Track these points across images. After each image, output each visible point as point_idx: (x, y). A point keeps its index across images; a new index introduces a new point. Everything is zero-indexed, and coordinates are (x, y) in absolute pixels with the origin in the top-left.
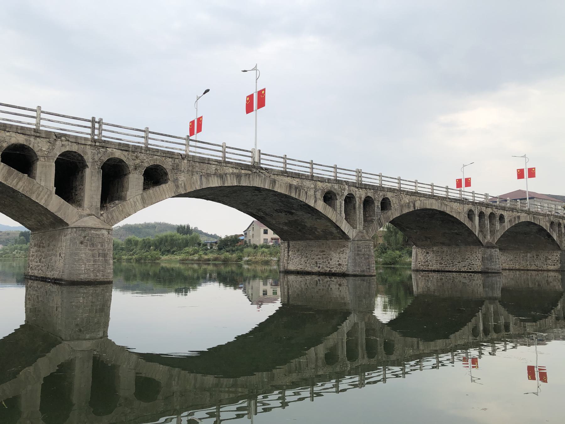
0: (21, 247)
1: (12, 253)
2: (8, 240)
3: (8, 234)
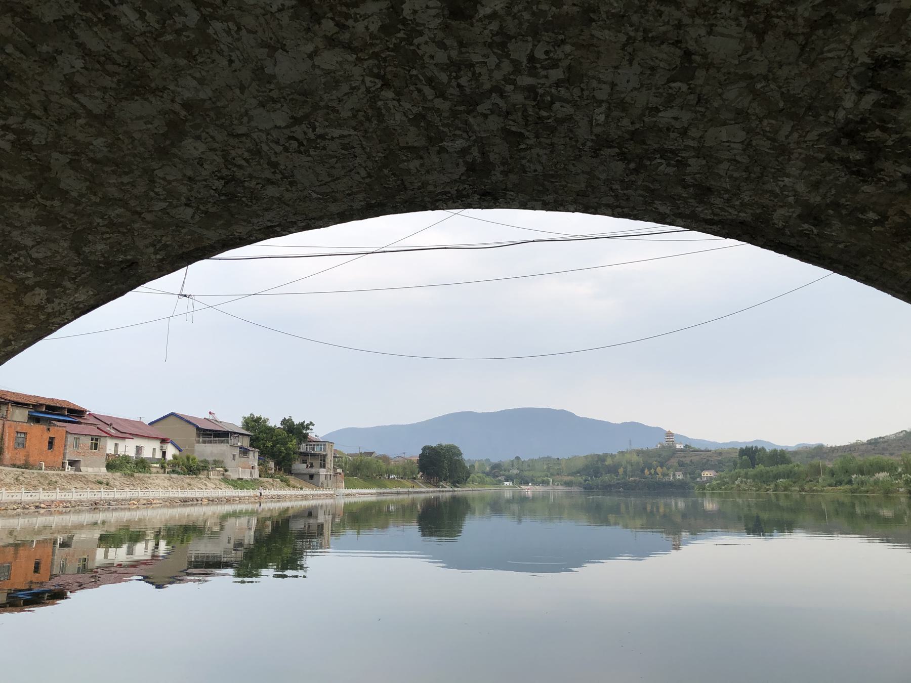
0: (746, 474)
1: (734, 483)
2: (720, 462)
3: (720, 454)
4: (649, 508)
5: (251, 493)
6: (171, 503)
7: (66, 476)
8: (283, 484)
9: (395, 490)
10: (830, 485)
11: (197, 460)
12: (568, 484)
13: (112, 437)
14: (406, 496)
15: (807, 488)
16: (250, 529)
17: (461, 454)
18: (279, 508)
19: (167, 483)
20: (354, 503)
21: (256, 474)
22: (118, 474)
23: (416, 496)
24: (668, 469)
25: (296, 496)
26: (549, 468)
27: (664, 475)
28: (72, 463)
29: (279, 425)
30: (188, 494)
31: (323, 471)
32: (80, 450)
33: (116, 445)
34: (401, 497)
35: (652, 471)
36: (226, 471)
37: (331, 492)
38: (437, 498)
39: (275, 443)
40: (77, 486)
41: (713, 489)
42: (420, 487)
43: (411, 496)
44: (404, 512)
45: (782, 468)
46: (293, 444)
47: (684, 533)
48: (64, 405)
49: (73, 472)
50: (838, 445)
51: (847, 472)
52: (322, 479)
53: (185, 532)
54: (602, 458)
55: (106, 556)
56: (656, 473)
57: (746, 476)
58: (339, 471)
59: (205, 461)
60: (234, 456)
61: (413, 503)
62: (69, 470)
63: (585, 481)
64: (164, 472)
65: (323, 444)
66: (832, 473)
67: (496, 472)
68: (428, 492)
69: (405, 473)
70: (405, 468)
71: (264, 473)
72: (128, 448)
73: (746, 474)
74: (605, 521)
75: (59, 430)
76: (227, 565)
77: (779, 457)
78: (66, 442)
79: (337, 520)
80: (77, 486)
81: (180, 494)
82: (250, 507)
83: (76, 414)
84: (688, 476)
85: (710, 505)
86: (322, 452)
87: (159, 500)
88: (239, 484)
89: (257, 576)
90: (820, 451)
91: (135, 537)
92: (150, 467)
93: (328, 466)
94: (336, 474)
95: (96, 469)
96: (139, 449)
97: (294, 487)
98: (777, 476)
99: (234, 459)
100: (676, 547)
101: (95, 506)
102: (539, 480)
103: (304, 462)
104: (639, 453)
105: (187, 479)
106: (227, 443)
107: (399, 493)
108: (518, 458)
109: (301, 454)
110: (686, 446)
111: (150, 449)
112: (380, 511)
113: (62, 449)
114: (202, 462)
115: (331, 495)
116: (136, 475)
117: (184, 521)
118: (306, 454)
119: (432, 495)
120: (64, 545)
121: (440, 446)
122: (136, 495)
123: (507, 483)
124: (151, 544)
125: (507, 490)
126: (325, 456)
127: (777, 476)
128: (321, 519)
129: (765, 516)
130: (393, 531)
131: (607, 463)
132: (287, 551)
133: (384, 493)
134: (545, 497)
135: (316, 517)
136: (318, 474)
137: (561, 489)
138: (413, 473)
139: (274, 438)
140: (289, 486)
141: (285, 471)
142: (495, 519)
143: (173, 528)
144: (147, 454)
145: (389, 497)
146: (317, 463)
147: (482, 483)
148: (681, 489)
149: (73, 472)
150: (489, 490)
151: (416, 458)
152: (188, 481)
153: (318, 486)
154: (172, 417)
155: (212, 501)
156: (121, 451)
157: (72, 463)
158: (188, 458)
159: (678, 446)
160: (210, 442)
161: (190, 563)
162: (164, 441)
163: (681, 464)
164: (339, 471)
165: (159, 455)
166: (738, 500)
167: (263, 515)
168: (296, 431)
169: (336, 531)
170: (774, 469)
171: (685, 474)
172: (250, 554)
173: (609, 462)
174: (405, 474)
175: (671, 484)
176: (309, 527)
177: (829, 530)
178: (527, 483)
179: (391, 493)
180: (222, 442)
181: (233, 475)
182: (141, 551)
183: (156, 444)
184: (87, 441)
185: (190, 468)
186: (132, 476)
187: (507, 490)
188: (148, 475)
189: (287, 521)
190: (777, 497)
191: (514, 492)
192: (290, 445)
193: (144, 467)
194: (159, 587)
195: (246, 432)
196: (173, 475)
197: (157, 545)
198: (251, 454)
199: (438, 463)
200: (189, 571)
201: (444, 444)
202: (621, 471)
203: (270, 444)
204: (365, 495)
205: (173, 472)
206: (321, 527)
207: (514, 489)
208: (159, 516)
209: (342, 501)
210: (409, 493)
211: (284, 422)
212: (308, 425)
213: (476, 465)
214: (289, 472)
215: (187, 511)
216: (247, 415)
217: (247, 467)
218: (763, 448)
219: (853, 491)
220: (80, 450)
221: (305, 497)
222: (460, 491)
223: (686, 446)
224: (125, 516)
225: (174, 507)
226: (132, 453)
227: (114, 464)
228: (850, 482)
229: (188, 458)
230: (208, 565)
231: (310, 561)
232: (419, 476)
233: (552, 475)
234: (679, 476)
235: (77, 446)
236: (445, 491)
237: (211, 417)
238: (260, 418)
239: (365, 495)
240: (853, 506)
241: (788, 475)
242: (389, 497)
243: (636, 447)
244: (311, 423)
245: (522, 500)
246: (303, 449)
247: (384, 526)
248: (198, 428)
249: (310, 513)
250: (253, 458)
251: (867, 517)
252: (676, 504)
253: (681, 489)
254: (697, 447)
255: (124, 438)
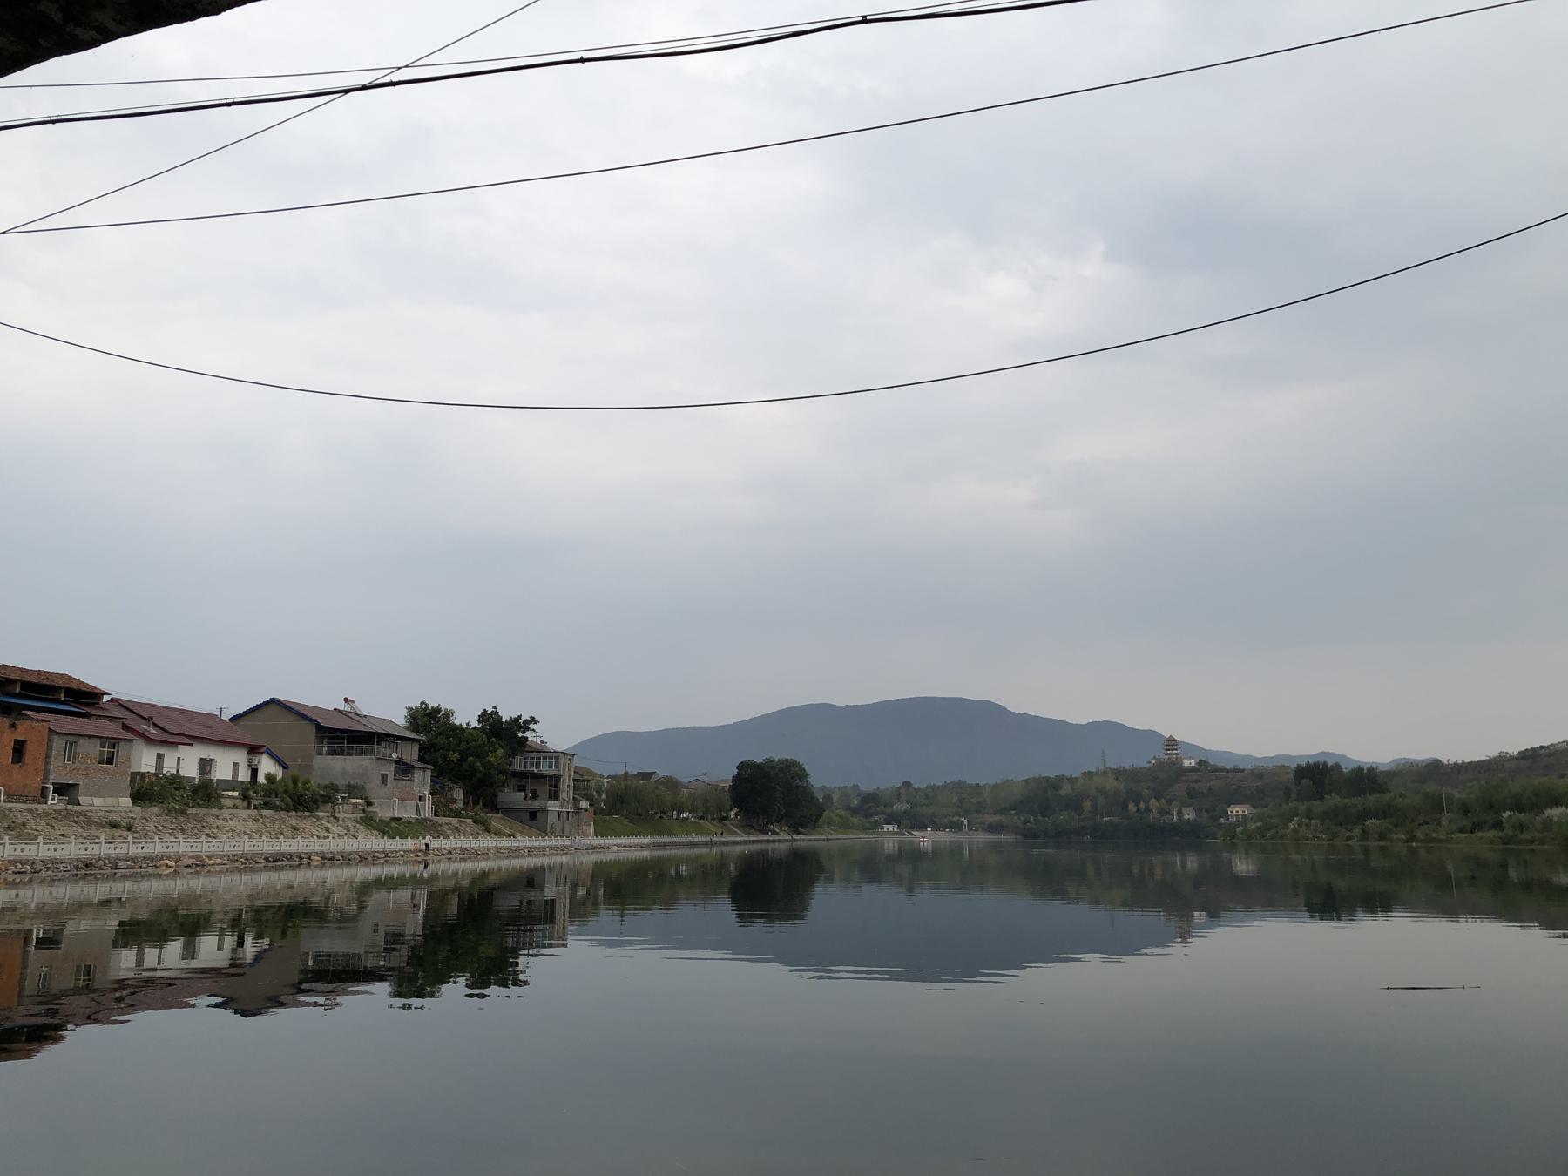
0: (1309, 810)
4: (1136, 869)
5: (410, 844)
6: (248, 863)
7: (46, 814)
8: (476, 828)
9: (685, 839)
10: (1461, 831)
11: (314, 785)
12: (994, 828)
13: (149, 740)
14: (705, 850)
15: (1419, 834)
16: (416, 907)
17: (806, 776)
18: (507, 870)
19: (251, 826)
20: (613, 863)
21: (427, 812)
22: (155, 810)
23: (725, 849)
24: (1169, 802)
25: (498, 850)
26: (961, 801)
27: (1163, 812)
28: (61, 789)
29: (474, 723)
30: (284, 846)
31: (553, 806)
32: (77, 766)
33: (160, 757)
34: (697, 851)
35: (1142, 806)
36: (369, 804)
37: (567, 842)
38: (764, 854)
39: (465, 754)
40: (66, 831)
41: (1250, 838)
42: (734, 834)
43: (715, 849)
44: (705, 878)
45: (1372, 800)
46: (497, 755)
47: (1196, 914)
48: (59, 683)
49: (62, 806)
50: (1467, 760)
51: (1493, 806)
52: (552, 819)
53: (291, 915)
54: (1055, 784)
55: (140, 961)
56: (1148, 810)
57: (1309, 814)
58: (584, 804)
59: (334, 788)
60: (385, 777)
61: (722, 863)
62: (54, 802)
63: (1025, 823)
64: (248, 807)
65: (556, 755)
66: (1465, 809)
67: (870, 808)
68: (746, 842)
69: (708, 807)
70: (706, 800)
71: (443, 806)
72: (186, 762)
73: (1309, 810)
74: (1060, 893)
75: (33, 728)
76: (372, 976)
77: (1366, 780)
78: (50, 748)
79: (581, 892)
80: (66, 831)
81: (267, 846)
82: (408, 870)
83: (82, 698)
84: (1205, 815)
85: (1242, 866)
86: (553, 771)
87: (234, 857)
88: (394, 828)
89: (432, 995)
90: (1434, 770)
91: (191, 926)
92: (220, 796)
93: (563, 795)
94: (578, 811)
95: (111, 801)
96: (205, 764)
97: (499, 833)
98: (1365, 815)
99: (384, 782)
100: (1184, 936)
101: (85, 869)
102: (945, 821)
103: (521, 788)
104: (1119, 773)
105: (293, 819)
106: (372, 753)
107: (693, 845)
108: (907, 784)
109: (514, 774)
110: (1201, 762)
111: (227, 765)
112: (661, 876)
113: (41, 764)
114: (325, 787)
115: (569, 848)
116: (190, 811)
117: (286, 897)
118: (524, 775)
119: (758, 847)
120: (46, 943)
121: (769, 761)
122: (173, 849)
123: (890, 828)
124: (230, 942)
125: (890, 838)
126: (558, 778)
127: (1365, 815)
128: (550, 891)
129: (1341, 884)
130: (688, 913)
131: (1063, 792)
132: (488, 950)
133: (664, 845)
134: (955, 851)
135: (542, 888)
136: (545, 810)
137: (983, 837)
138: (720, 809)
139: (463, 746)
140: (488, 831)
141: (485, 806)
142: (868, 889)
143: (267, 908)
144: (222, 772)
145: (674, 852)
146: (543, 790)
147: (846, 826)
148: (1191, 837)
149: (62, 806)
150: (857, 839)
151: (727, 784)
152: (294, 822)
153: (543, 831)
154: (272, 706)
155: (329, 859)
156: (169, 767)
157: (61, 789)
158: (295, 781)
159: (1186, 763)
160: (341, 752)
161: (305, 971)
162: (253, 750)
163: (1192, 795)
164: (584, 804)
165: (244, 775)
166: (1293, 856)
167: (440, 884)
168: (504, 733)
169: (581, 911)
170: (1359, 802)
171: (1198, 811)
172: (416, 958)
173: (1066, 790)
174: (707, 811)
175: (1174, 829)
176: (530, 902)
177: (1451, 910)
178: (923, 827)
179: (679, 844)
180: (362, 753)
181: (382, 812)
182: (211, 950)
183: (240, 756)
184: (91, 750)
185: (296, 798)
186: (183, 812)
187: (890, 838)
188: (214, 811)
189: (488, 895)
190: (1366, 851)
191: (900, 842)
192: (491, 758)
193: (208, 797)
194: (246, 1013)
195: (412, 735)
196: (265, 812)
197: (241, 943)
198: (417, 775)
199: (766, 789)
200: (304, 986)
201: (776, 758)
202: (1087, 805)
203: (455, 756)
204: (632, 847)
205: (266, 805)
206: (551, 904)
207: (902, 838)
208: (236, 888)
209: (591, 859)
210: (711, 844)
211: (485, 717)
212: (526, 722)
213: (836, 797)
214: (493, 805)
215: (282, 878)
216: (415, 704)
217: (410, 798)
218: (1337, 766)
219: (1507, 841)
220: (77, 766)
221: (515, 852)
222: (805, 840)
223: (1201, 762)
224: (178, 886)
225: (253, 870)
226: (190, 770)
227: (146, 791)
228: (1498, 825)
229: (295, 781)
230: (339, 975)
231: (535, 965)
232: (732, 814)
233: (967, 813)
234: (1189, 814)
235: (72, 757)
236: (779, 841)
237: (348, 708)
238: (437, 710)
239: (632, 847)
240: (1504, 866)
241: (1384, 812)
242: (674, 852)
243: (1112, 764)
244: (533, 720)
245: (915, 856)
246: (518, 765)
247: (669, 903)
248: (319, 728)
249: (531, 880)
250: (422, 782)
251: (1527, 887)
252: (1184, 865)
253: (1191, 837)
254: (1220, 764)
255: (174, 745)
